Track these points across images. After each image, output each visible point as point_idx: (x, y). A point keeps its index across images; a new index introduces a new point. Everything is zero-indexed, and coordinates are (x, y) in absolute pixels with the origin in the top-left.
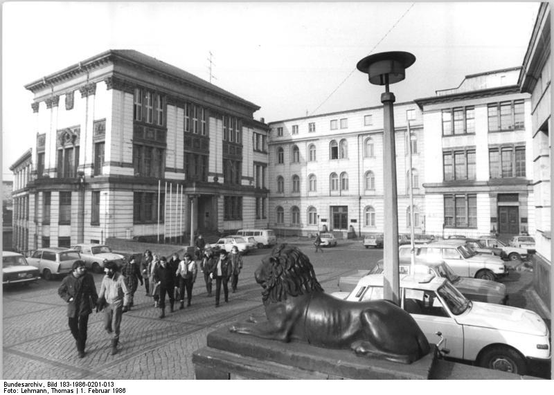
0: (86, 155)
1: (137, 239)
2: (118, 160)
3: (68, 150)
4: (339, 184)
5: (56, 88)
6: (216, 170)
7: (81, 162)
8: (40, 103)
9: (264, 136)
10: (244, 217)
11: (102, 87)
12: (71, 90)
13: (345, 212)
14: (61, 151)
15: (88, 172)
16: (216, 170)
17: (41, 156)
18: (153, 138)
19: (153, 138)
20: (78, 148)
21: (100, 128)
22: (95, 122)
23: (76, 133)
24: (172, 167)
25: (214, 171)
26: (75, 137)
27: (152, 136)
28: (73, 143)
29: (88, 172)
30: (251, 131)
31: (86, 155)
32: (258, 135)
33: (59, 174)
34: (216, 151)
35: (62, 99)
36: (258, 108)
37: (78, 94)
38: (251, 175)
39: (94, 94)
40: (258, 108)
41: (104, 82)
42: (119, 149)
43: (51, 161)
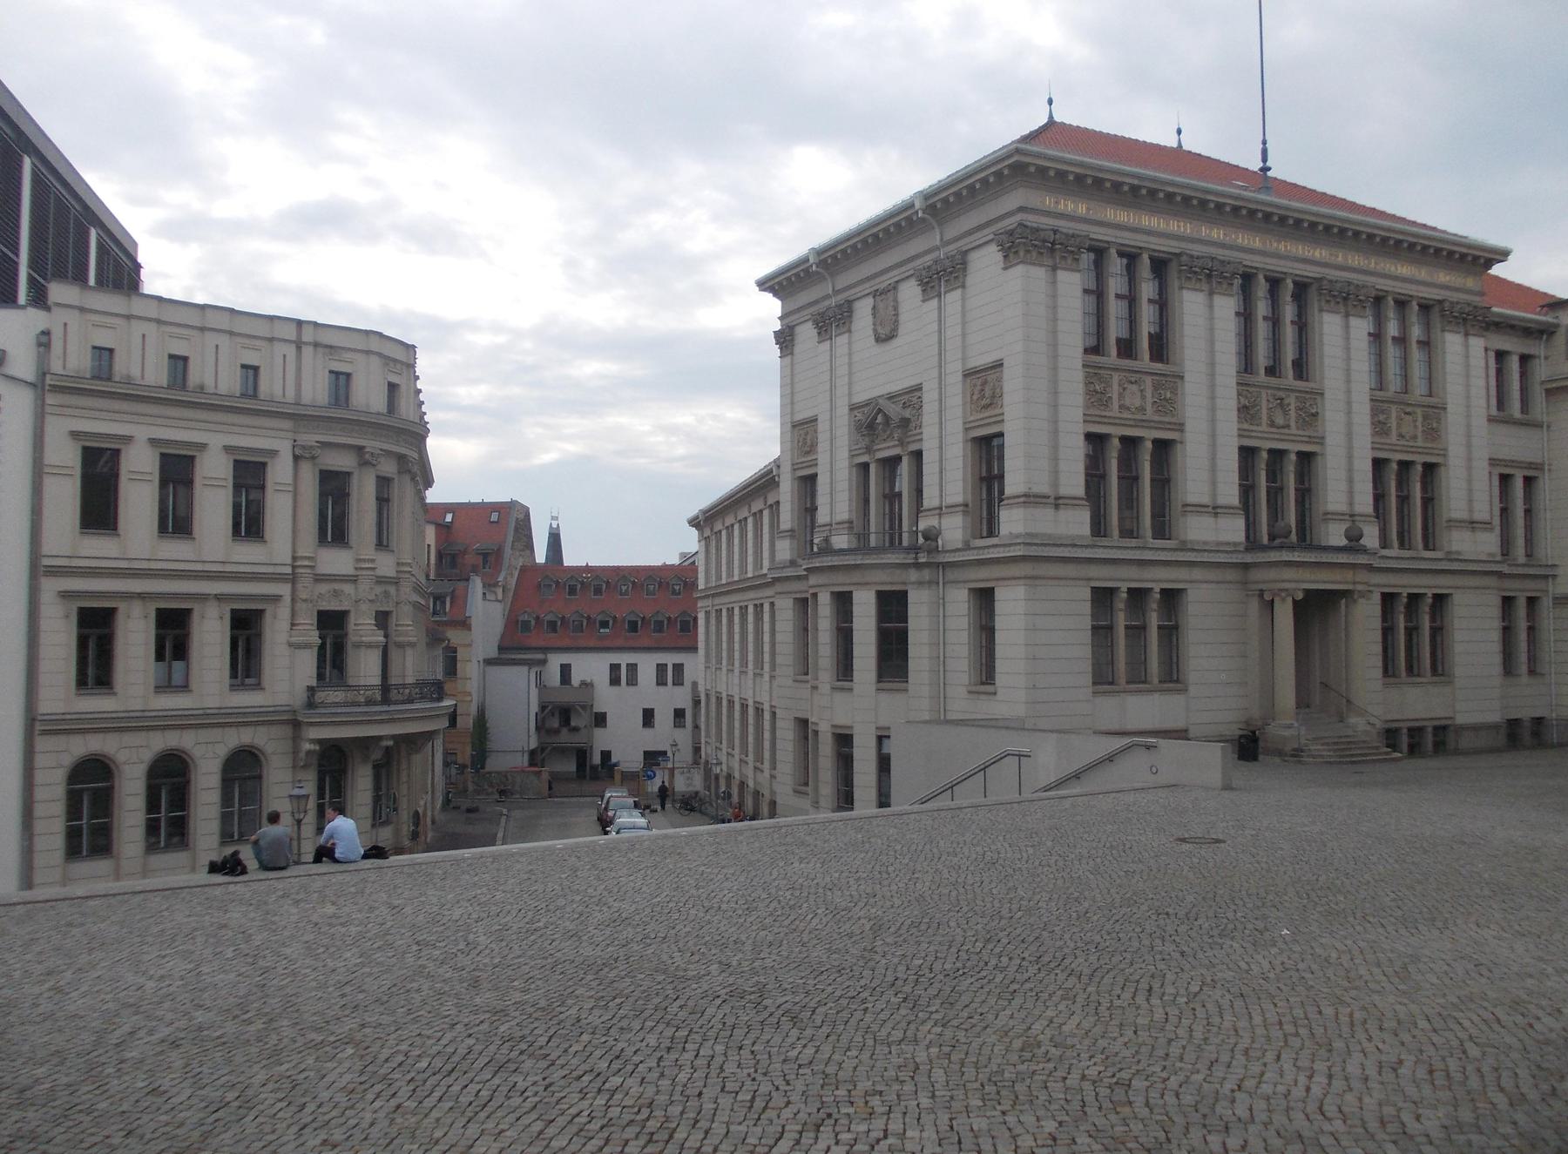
0: (947, 475)
1: (153, 840)
2: (1043, 488)
3: (892, 463)
4: (1082, 209)
5: (843, 280)
6: (1471, 511)
7: (930, 498)
8: (798, 330)
9: (1525, 359)
10: (1458, 671)
11: (986, 262)
12: (883, 282)
13: (618, 777)
14: (865, 467)
15: (953, 530)
16: (1471, 511)
17: (808, 483)
18: (1142, 409)
19: (1142, 409)
20: (918, 455)
21: (984, 382)
22: (968, 374)
23: (907, 413)
24: (1206, 500)
25: (1343, 508)
26: (905, 423)
27: (1138, 403)
28: (902, 443)
29: (953, 530)
30: (1477, 344)
31: (947, 475)
32: (1501, 356)
33: (863, 536)
34: (1469, 469)
35: (864, 309)
36: (1502, 255)
37: (910, 292)
38: (1485, 516)
39: (963, 286)
40: (1502, 255)
41: (993, 248)
42: (1045, 452)
43: (836, 501)
